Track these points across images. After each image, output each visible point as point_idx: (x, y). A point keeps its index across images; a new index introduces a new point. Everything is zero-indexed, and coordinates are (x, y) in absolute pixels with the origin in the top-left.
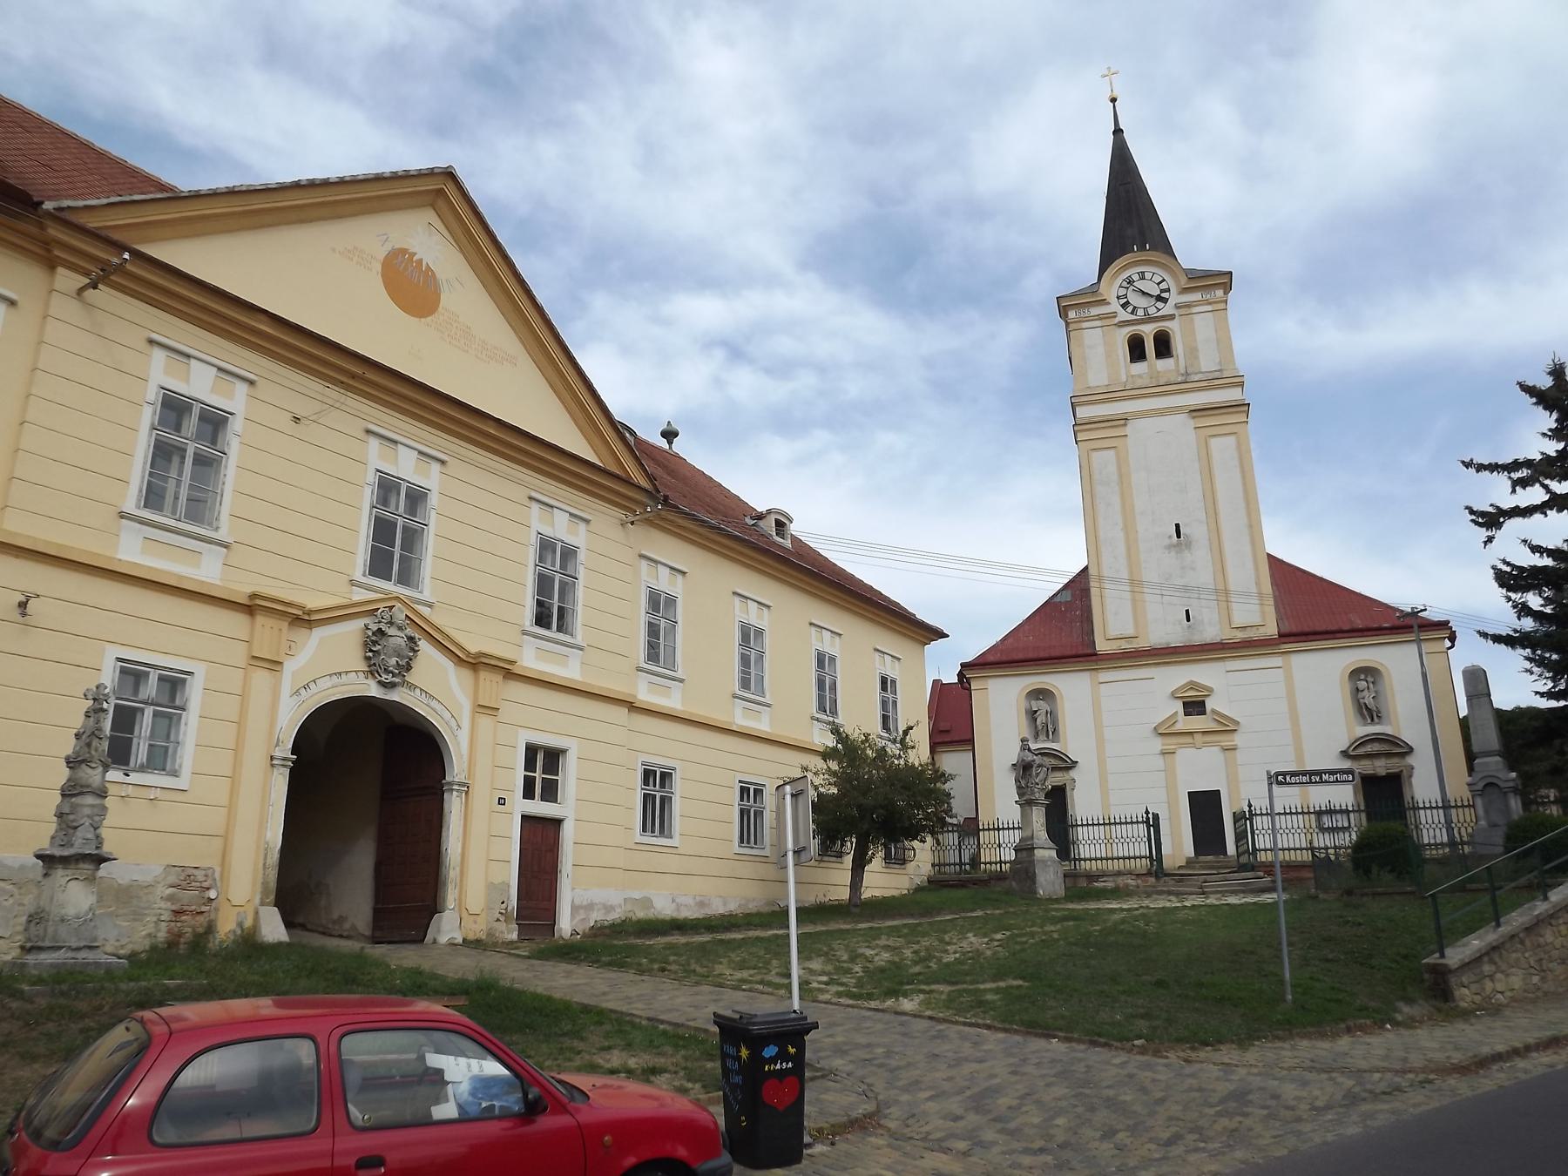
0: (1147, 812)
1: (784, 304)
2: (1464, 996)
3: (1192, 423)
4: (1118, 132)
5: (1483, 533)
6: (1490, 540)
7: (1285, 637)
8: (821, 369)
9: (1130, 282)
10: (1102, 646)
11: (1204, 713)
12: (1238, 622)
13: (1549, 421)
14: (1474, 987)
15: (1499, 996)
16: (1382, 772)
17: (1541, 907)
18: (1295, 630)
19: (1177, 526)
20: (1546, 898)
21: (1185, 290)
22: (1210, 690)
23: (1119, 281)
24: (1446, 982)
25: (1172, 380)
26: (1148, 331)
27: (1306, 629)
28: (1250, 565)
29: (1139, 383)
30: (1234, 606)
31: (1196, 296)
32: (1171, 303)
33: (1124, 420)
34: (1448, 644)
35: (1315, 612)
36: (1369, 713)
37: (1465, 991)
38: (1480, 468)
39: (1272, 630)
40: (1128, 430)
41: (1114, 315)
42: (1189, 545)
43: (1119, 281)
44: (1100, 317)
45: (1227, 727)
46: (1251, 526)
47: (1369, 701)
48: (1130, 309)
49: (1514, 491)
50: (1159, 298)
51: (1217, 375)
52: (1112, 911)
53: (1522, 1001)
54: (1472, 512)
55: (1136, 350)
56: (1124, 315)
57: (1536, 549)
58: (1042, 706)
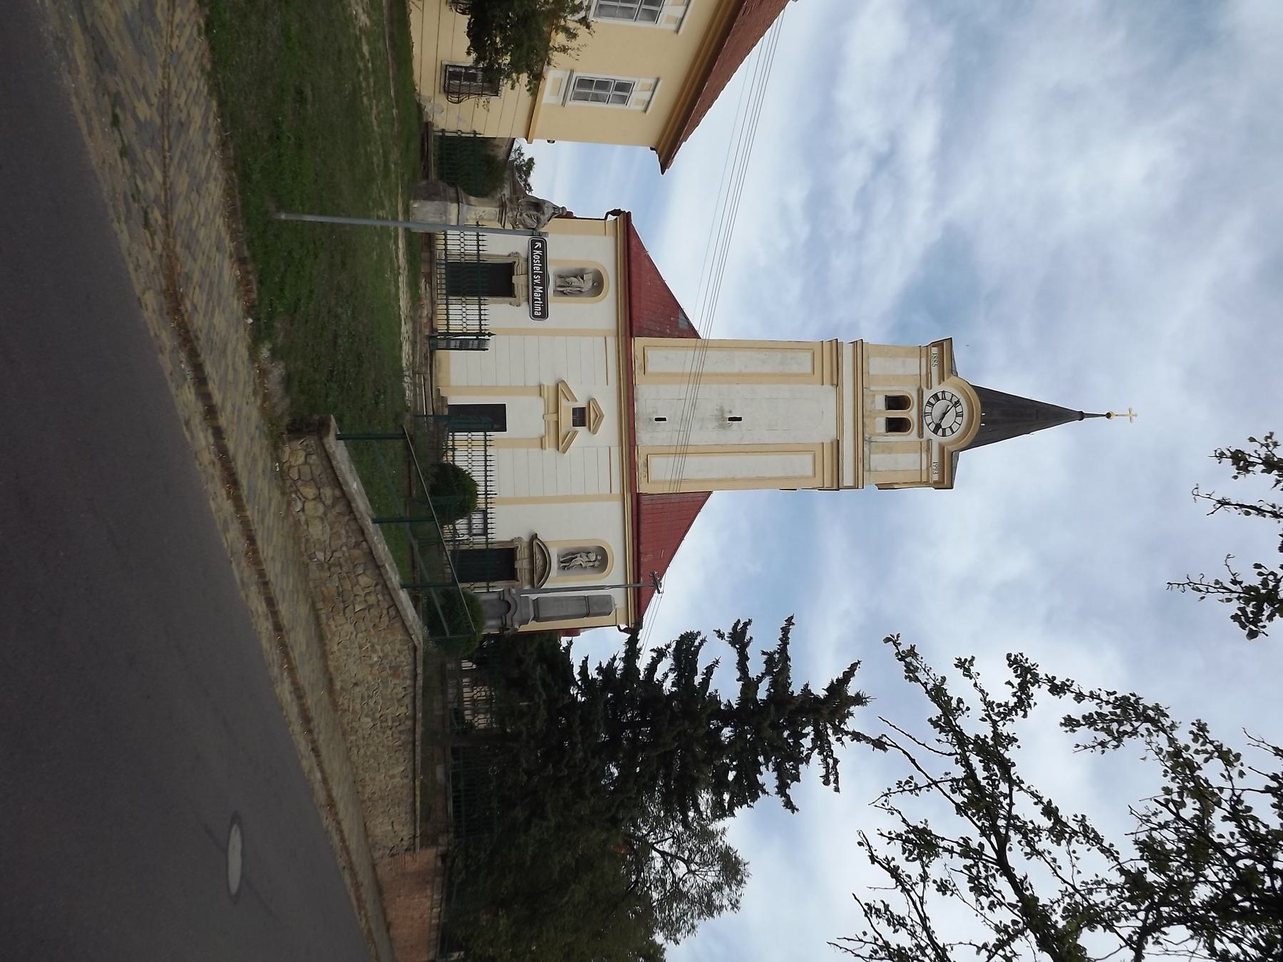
0: (490, 335)
1: (919, 208)
2: (296, 454)
3: (827, 441)
4: (1082, 416)
5: (727, 630)
6: (721, 636)
7: (637, 499)
8: (860, 236)
9: (957, 403)
10: (639, 343)
11: (574, 425)
12: (654, 461)
13: (820, 690)
14: (306, 469)
15: (299, 506)
16: (518, 565)
17: (395, 579)
18: (643, 507)
19: (740, 419)
20: (403, 587)
21: (942, 449)
22: (595, 432)
23: (959, 396)
24: (310, 433)
25: (867, 429)
26: (911, 414)
27: (642, 517)
28: (700, 476)
29: (868, 401)
30: (671, 459)
31: (935, 458)
32: (933, 436)
33: (837, 384)
34: (623, 627)
35: (656, 526)
36: (568, 560)
37: (301, 460)
38: (785, 631)
39: (644, 488)
40: (828, 387)
41: (929, 386)
42: (722, 427)
43: (959, 396)
44: (929, 373)
45: (561, 443)
46: (734, 479)
47: (579, 561)
48: (932, 401)
49: (764, 653)
50: (938, 426)
51: (867, 467)
52: (396, 244)
53: (296, 531)
54: (746, 624)
55: (896, 402)
56: (927, 395)
57: (709, 671)
58: (587, 285)
